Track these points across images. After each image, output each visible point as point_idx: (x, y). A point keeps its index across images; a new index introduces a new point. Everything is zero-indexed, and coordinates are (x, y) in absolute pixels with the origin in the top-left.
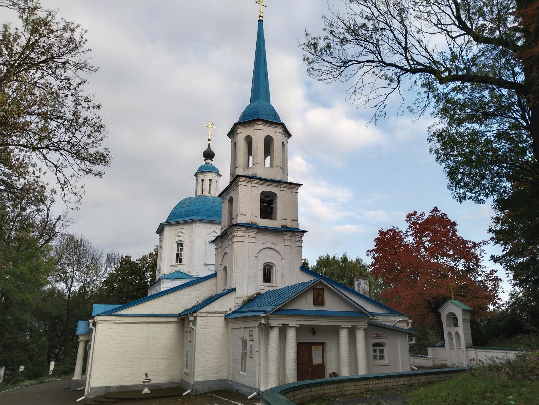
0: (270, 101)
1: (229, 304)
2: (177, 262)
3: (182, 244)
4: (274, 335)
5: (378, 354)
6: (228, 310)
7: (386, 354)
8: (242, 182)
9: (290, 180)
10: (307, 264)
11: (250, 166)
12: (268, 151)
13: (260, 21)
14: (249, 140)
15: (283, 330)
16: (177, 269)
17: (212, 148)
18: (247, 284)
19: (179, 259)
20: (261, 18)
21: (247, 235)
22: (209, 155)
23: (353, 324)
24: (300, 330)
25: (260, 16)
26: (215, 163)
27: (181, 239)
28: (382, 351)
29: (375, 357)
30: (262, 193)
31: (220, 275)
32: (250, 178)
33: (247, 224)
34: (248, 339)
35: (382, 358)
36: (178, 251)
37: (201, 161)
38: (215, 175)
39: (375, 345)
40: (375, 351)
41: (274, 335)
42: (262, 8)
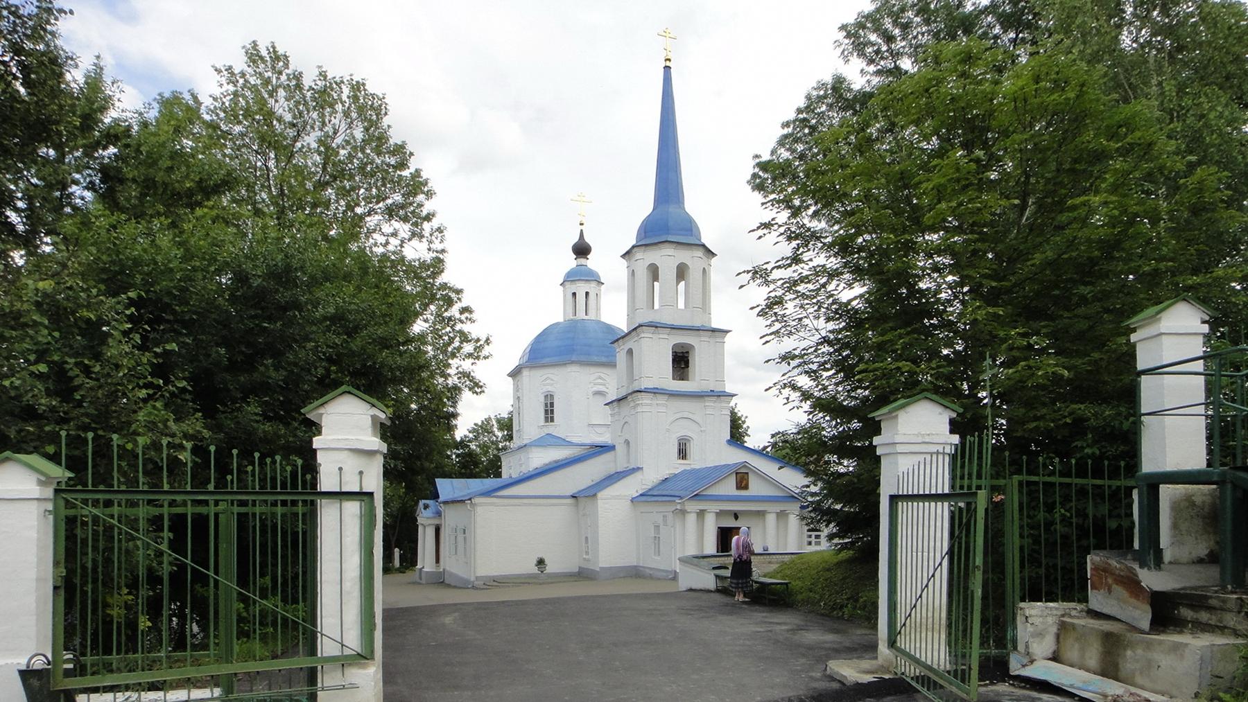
1: (631, 487)
2: (546, 420)
3: (552, 396)
4: (691, 519)
5: (813, 539)
9: (714, 325)
11: (656, 306)
13: (667, 68)
14: (654, 272)
15: (701, 514)
16: (546, 431)
17: (587, 239)
18: (658, 465)
19: (549, 414)
20: (668, 64)
21: (655, 402)
22: (582, 250)
24: (720, 514)
26: (592, 262)
27: (550, 388)
31: (620, 449)
32: (655, 326)
37: (571, 262)
38: (593, 284)
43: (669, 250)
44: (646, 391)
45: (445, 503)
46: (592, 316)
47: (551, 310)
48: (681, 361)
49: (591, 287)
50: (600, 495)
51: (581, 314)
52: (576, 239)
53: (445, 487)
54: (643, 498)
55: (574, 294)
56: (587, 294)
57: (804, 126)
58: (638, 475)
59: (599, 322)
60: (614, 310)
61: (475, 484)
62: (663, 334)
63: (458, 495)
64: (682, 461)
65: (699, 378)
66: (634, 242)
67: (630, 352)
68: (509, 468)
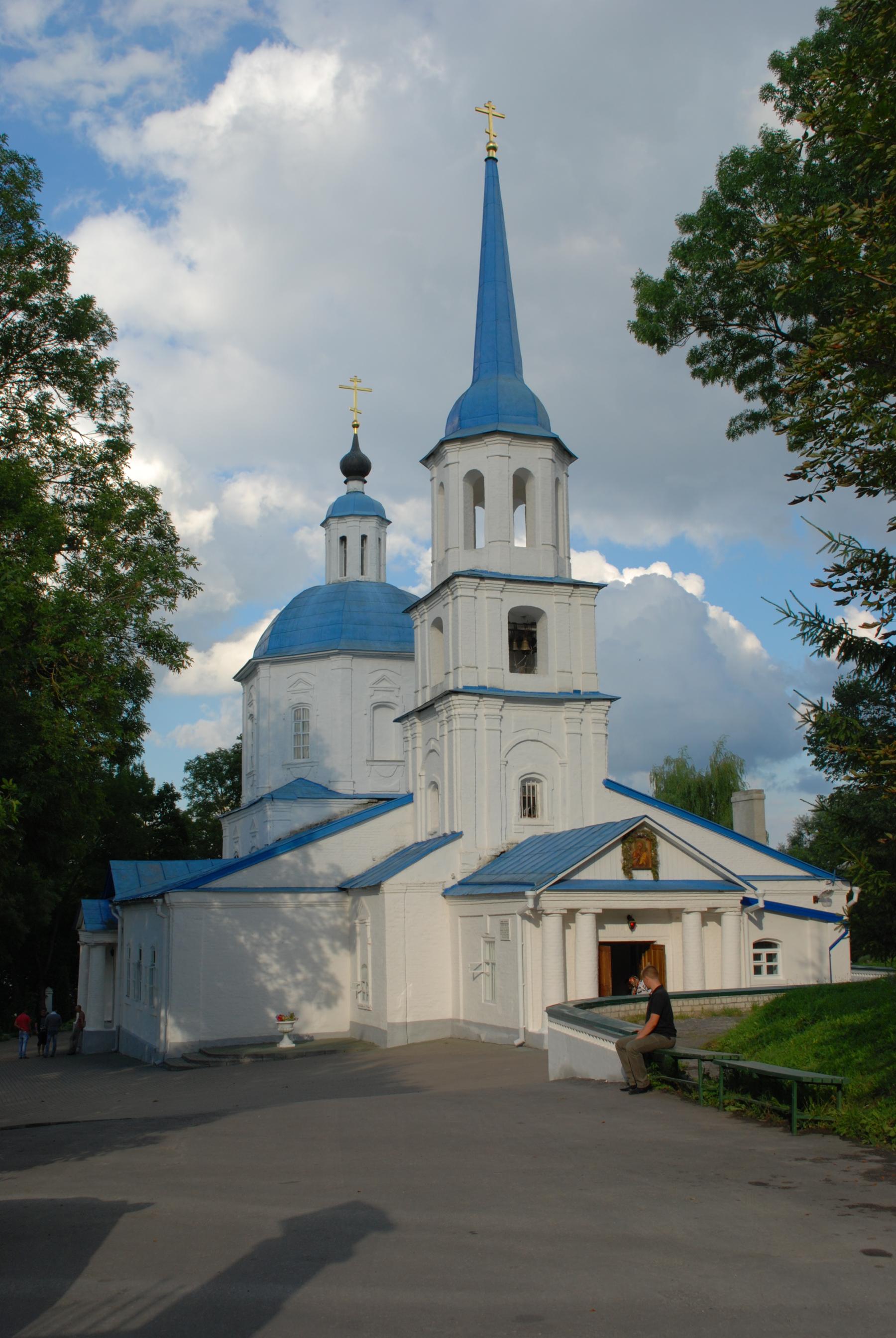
0: (521, 372)
1: (454, 863)
4: (552, 924)
5: (764, 963)
6: (449, 878)
7: (779, 962)
8: (464, 587)
9: (576, 576)
10: (736, 387)
11: (480, 543)
12: (519, 495)
14: (476, 483)
15: (569, 917)
17: (364, 449)
18: (490, 830)
20: (493, 154)
22: (356, 467)
23: (711, 904)
25: (489, 149)
26: (373, 487)
27: (303, 698)
28: (771, 957)
29: (757, 970)
30: (513, 613)
33: (480, 687)
34: (498, 937)
35: (771, 970)
36: (296, 729)
37: (336, 486)
39: (758, 945)
40: (757, 957)
41: (552, 924)
42: (494, 125)
43: (496, 446)
44: (466, 692)
45: (126, 903)
46: (371, 575)
47: (312, 560)
48: (523, 640)
49: (369, 526)
50: (387, 886)
51: (353, 574)
52: (347, 449)
53: (127, 875)
54: (467, 890)
55: (343, 539)
56: (364, 538)
57: (715, 226)
58: (459, 843)
59: (385, 585)
60: (409, 552)
61: (178, 869)
62: (488, 592)
63: (149, 887)
64: (527, 820)
65: (556, 667)
66: (442, 435)
67: (438, 624)
68: (236, 839)
